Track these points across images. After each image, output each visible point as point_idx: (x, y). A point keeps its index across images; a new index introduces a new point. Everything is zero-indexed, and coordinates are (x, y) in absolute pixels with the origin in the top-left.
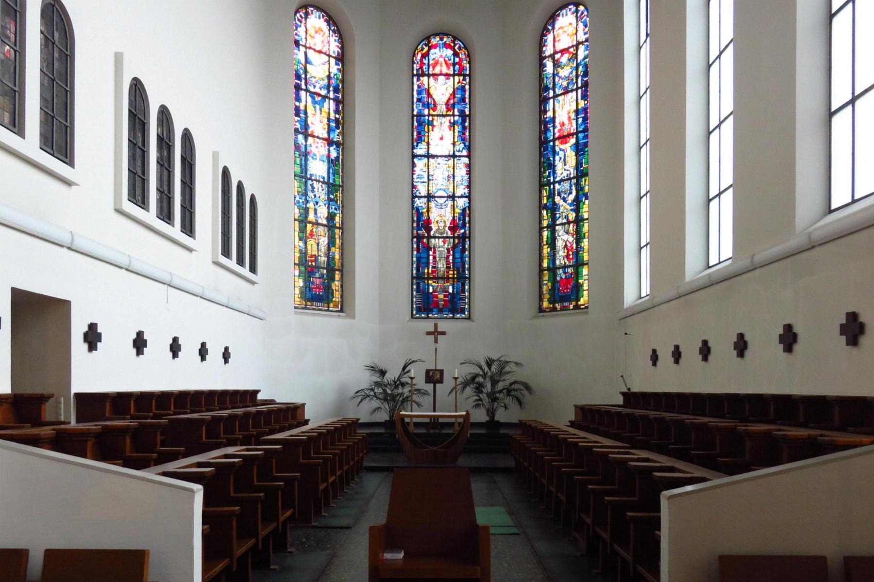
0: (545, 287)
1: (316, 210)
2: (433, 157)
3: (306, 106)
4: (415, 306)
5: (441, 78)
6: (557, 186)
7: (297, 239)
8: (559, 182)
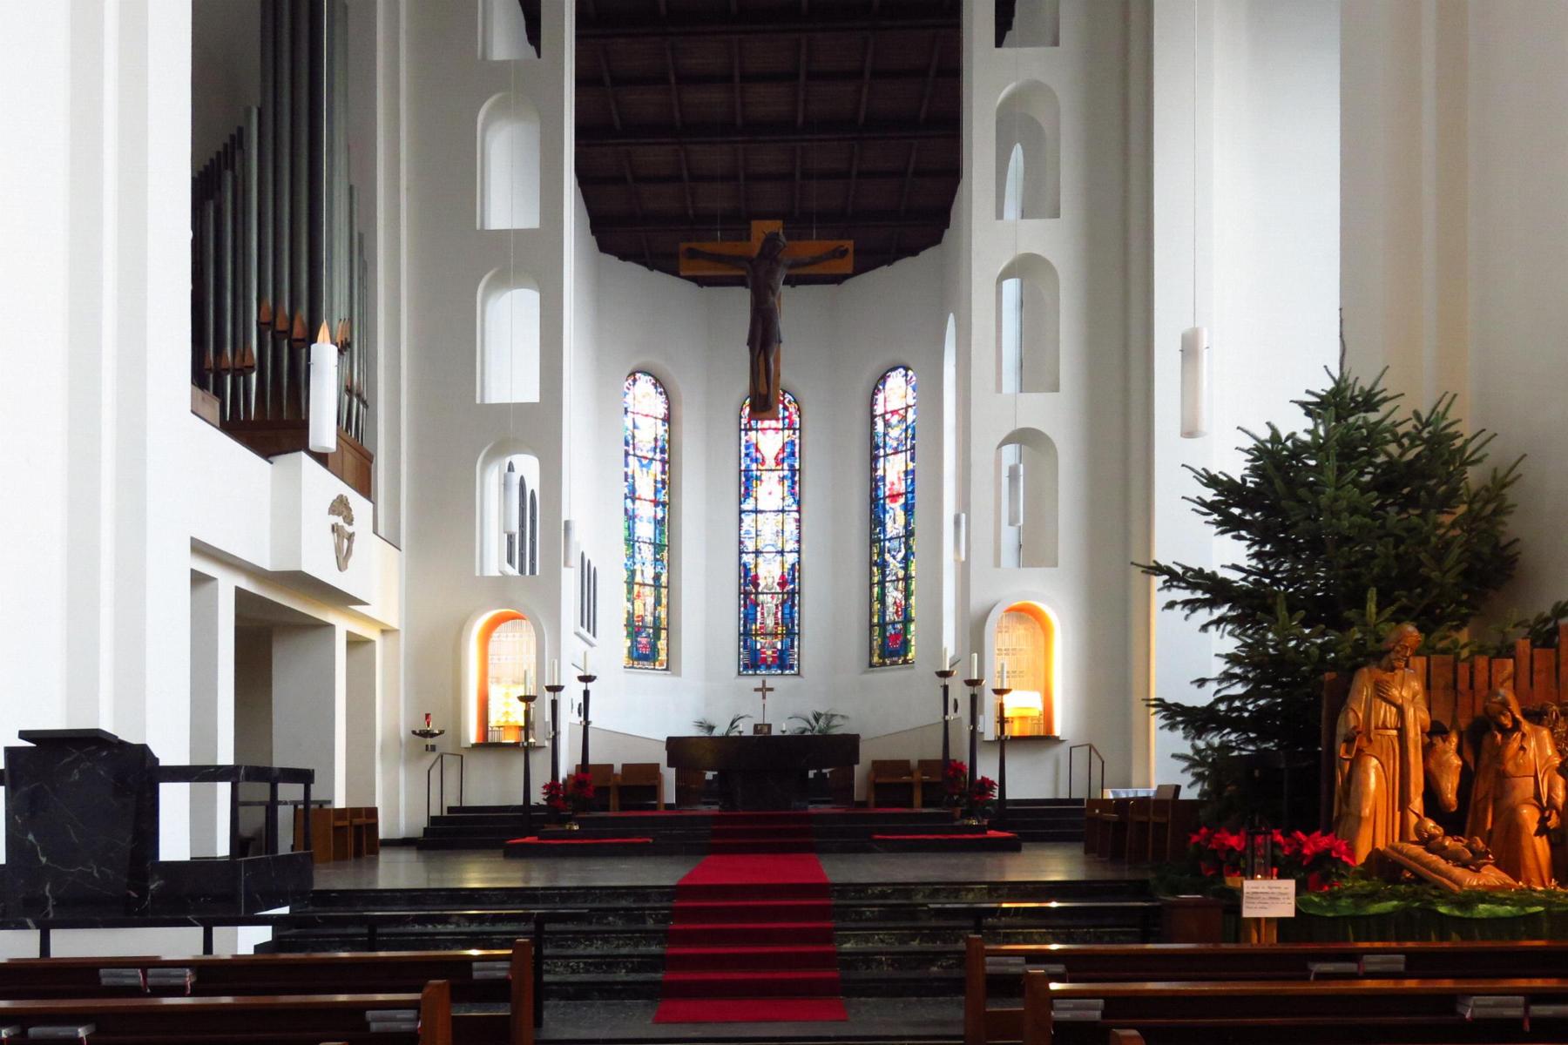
0: (875, 643)
1: (642, 571)
2: (761, 512)
3: (634, 472)
4: (742, 663)
5: (770, 433)
6: (887, 544)
7: (625, 600)
8: (890, 540)
